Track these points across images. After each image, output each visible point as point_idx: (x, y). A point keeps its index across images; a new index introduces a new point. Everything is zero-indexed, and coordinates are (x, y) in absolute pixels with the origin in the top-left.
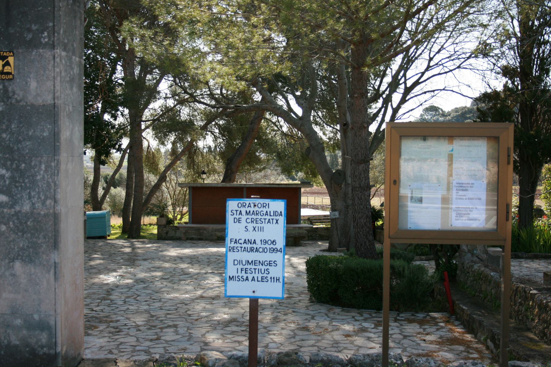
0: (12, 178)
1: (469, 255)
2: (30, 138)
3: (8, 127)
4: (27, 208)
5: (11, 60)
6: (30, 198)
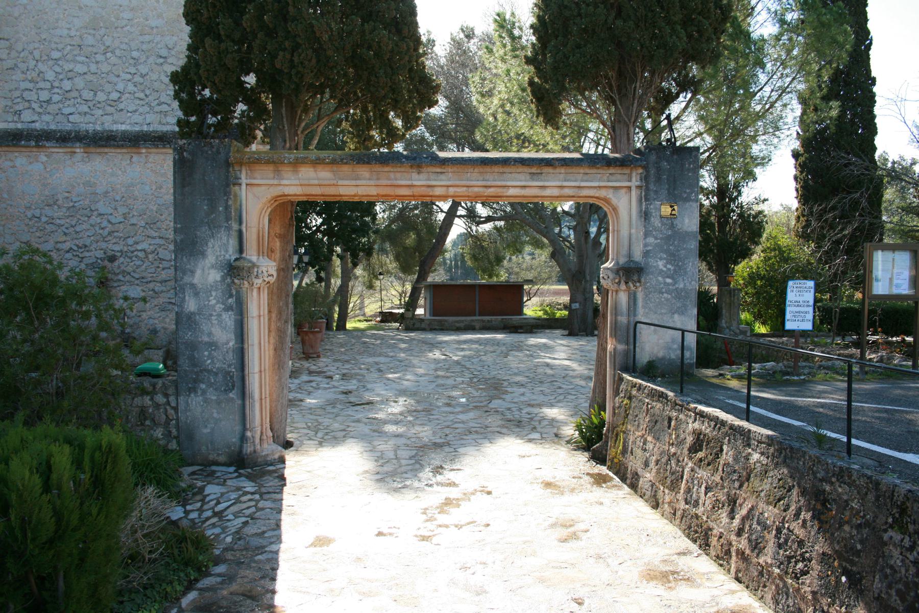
0: (675, 270)
1: (728, 330)
2: (684, 249)
3: (673, 243)
4: (681, 286)
5: (676, 207)
6: (683, 280)
